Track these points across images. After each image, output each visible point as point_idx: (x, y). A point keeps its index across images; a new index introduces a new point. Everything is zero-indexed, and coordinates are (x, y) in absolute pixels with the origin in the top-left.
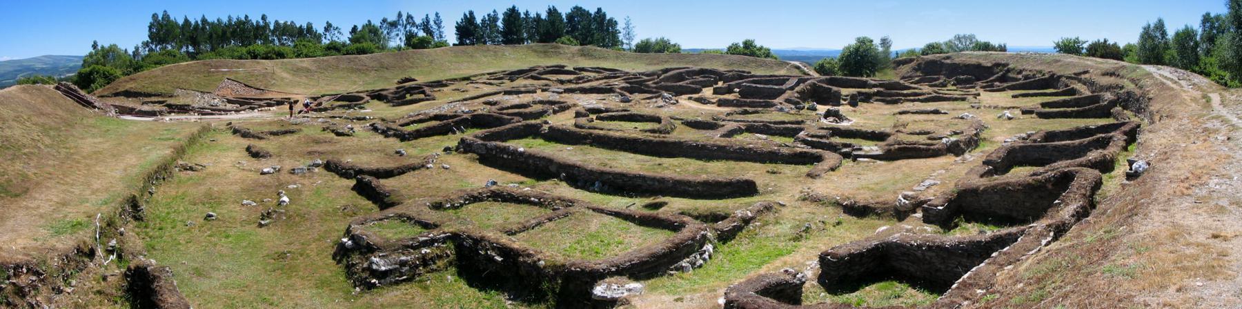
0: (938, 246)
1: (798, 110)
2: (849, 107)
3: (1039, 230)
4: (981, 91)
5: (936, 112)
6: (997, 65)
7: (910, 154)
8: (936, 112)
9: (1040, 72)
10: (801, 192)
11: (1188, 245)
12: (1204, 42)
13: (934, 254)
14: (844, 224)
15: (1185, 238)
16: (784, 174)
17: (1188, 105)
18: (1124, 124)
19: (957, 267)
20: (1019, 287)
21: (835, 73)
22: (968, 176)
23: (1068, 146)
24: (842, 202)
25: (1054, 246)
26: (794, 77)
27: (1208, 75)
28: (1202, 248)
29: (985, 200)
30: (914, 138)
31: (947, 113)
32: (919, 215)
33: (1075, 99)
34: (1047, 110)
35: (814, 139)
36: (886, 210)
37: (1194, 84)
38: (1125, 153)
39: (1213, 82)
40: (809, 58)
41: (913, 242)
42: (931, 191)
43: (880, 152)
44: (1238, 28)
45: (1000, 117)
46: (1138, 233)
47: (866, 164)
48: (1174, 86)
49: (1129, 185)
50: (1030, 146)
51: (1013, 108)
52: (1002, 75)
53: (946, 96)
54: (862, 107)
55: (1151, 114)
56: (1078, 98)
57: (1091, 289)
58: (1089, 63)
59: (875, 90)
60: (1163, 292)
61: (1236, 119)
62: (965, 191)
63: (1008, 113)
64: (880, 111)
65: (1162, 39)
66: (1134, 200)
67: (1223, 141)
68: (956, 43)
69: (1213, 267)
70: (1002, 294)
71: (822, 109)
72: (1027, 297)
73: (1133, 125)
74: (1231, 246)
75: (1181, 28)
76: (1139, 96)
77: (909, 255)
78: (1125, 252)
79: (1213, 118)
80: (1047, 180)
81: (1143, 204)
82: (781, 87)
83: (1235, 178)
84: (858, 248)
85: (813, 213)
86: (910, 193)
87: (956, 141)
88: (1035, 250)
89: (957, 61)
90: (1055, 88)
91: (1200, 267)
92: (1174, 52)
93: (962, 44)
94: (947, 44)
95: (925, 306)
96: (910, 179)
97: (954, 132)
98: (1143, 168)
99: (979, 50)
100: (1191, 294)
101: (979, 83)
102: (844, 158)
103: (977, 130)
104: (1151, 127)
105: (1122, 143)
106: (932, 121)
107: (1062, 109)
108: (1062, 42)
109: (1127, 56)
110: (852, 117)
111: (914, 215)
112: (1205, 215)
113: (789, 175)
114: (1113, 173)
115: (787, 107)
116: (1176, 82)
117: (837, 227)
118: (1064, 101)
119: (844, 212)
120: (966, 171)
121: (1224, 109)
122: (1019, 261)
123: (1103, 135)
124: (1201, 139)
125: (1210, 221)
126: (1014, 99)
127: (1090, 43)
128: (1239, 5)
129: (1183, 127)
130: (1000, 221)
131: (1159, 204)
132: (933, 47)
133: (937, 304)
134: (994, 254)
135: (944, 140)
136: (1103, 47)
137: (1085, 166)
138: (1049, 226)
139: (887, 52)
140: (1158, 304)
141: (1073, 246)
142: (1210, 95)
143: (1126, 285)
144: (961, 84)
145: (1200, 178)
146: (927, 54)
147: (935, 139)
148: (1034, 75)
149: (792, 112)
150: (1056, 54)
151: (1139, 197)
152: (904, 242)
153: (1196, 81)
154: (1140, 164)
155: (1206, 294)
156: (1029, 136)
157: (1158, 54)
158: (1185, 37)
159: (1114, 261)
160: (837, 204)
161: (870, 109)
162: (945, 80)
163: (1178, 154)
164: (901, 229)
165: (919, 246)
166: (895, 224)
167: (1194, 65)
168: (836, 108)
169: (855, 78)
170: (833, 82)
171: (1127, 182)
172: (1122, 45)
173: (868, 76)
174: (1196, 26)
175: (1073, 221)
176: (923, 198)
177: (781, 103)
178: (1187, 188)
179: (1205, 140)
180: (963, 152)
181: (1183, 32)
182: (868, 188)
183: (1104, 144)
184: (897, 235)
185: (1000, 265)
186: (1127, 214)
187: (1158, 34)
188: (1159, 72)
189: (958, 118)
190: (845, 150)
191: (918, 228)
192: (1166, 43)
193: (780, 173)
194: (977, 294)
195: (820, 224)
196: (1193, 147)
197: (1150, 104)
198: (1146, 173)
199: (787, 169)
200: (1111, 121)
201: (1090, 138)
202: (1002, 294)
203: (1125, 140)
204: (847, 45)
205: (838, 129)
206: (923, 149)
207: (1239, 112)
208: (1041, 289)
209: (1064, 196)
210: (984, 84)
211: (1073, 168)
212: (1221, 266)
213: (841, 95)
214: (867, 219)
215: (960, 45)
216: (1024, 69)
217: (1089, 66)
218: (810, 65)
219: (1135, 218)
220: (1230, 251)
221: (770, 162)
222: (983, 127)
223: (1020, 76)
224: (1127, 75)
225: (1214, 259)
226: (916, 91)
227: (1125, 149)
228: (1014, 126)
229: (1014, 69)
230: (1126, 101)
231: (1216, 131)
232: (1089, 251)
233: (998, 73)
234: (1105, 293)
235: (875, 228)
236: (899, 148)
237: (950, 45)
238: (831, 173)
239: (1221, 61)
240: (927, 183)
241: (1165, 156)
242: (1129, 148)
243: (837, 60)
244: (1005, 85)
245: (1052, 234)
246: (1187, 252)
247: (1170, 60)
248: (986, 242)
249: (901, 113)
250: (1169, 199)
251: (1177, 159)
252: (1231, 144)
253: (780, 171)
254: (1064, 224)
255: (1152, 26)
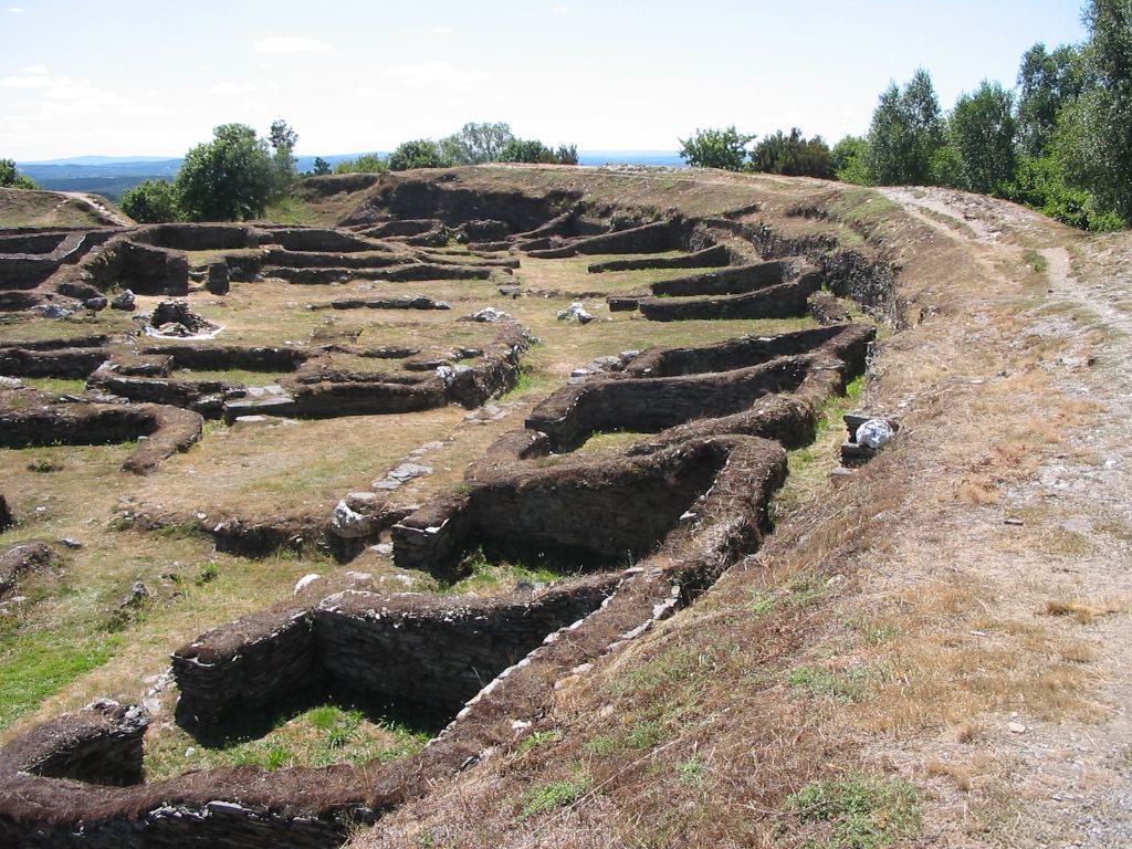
0: (427, 621)
1: (89, 311)
2: (208, 295)
3: (649, 580)
4: (522, 257)
5: (424, 305)
6: (557, 195)
7: (365, 403)
8: (424, 305)
9: (651, 211)
10: (115, 510)
11: (990, 627)
12: (1029, 120)
13: (418, 639)
14: (221, 578)
15: (982, 611)
16: (71, 469)
17: (989, 281)
18: (836, 331)
19: (469, 669)
20: (604, 713)
21: (171, 216)
22: (494, 455)
23: (711, 384)
24: (211, 525)
25: (681, 618)
26: (75, 230)
27: (1038, 202)
28: (1025, 636)
29: (531, 511)
30: (375, 366)
31: (447, 308)
32: (385, 547)
33: (727, 274)
34: (666, 300)
35: (134, 380)
36: (308, 536)
37: (1004, 229)
38: (840, 401)
39: (1051, 220)
40: (109, 182)
41: (371, 612)
42: (413, 491)
43: (286, 399)
44: (1118, 73)
45: (562, 318)
46: (869, 593)
47: (258, 429)
48: (955, 235)
49: (848, 476)
50: (628, 384)
51: (592, 295)
52: (567, 219)
53: (446, 267)
54: (239, 292)
55: (901, 305)
56: (735, 272)
57: (762, 724)
58: (758, 187)
59: (267, 249)
60: (927, 740)
61: (1111, 312)
62: (486, 489)
63: (580, 309)
64: (280, 301)
65: (927, 121)
66: (860, 514)
67: (1077, 370)
68: (468, 143)
69: (1052, 687)
70: (567, 730)
71: (147, 304)
72: (621, 738)
73: (858, 333)
74: (1097, 637)
75: (972, 89)
76: (871, 261)
77: (363, 641)
78: (838, 638)
79: (1051, 310)
80: (667, 465)
81: (881, 523)
82: (46, 256)
83: (1109, 463)
84: (257, 631)
85: (149, 559)
86: (366, 496)
87: (467, 373)
88: (639, 629)
89: (470, 184)
90: (683, 249)
91: (1018, 685)
92: (954, 151)
93: (480, 146)
94: (446, 144)
95: (399, 761)
96: (364, 463)
97: (462, 351)
98: (882, 437)
99: (518, 159)
100: (997, 752)
101: (518, 237)
102: (206, 419)
103: (512, 347)
104: (898, 337)
105: (832, 378)
106: (415, 325)
107: (698, 298)
108: (699, 141)
109: (844, 167)
110: (217, 318)
111: (375, 548)
112: (1030, 555)
113: (82, 471)
114: (812, 449)
115: (65, 305)
116: (958, 226)
117: (206, 585)
118: (704, 279)
119: (219, 549)
120: (489, 443)
121: (1081, 287)
122: (604, 653)
123: (790, 359)
124: (1021, 364)
125: (1041, 572)
126: (593, 275)
127: (760, 139)
128: (1120, 18)
129: (977, 335)
130: (563, 561)
131: (918, 524)
132: (418, 152)
133: (425, 756)
134: (550, 638)
135: (441, 371)
136: (790, 148)
137: (749, 431)
138: (670, 572)
139: (285, 159)
140: (917, 768)
141: (721, 621)
142: (1046, 253)
143: (841, 718)
144: (477, 241)
145: (1017, 461)
146: (404, 168)
147: (420, 368)
148: (636, 219)
149: (78, 316)
150: (685, 169)
151: (870, 507)
152: (352, 612)
153: (1008, 219)
154: (873, 428)
155: (1033, 754)
156: (626, 361)
157: (916, 158)
158: (983, 110)
159: (814, 658)
160: (201, 531)
161: (256, 296)
162: (443, 231)
163: (965, 403)
164: (346, 581)
165: (386, 622)
166: (330, 570)
167: (1003, 180)
168: (179, 300)
169: (218, 224)
170: (165, 237)
171: (845, 471)
172: (832, 142)
173: (248, 217)
174: (1009, 80)
175: (722, 561)
176: (393, 507)
177: (49, 297)
178: (987, 488)
179: (1031, 368)
180: (483, 399)
181: (978, 101)
182: (268, 485)
183: (790, 379)
184: (335, 597)
185: (561, 662)
186: (844, 547)
187: (916, 111)
188: (919, 202)
189: (472, 319)
190: (206, 399)
191: (382, 579)
192: (935, 131)
193: (61, 469)
194: (514, 731)
195: (166, 584)
196: (1003, 383)
197: (898, 281)
198: (888, 450)
199: (78, 458)
200: (808, 324)
201: (761, 366)
202: (567, 730)
203: (839, 370)
204: (195, 146)
205: (188, 350)
206: (395, 392)
207: (1120, 293)
208: (651, 719)
209: (702, 503)
210: (529, 241)
211: (723, 437)
212: (1072, 688)
213: (189, 267)
214: (271, 559)
215: (475, 149)
216: (614, 206)
217: (757, 194)
218: (112, 198)
219: (862, 556)
220: (1095, 650)
221: (37, 444)
222: (524, 342)
223: (606, 222)
224: (844, 213)
225: (1054, 668)
226: (380, 254)
227: (840, 390)
228: (594, 339)
229: (593, 204)
230: (842, 276)
231: (1060, 343)
232: (758, 633)
233: (558, 214)
234: (794, 733)
235: (291, 579)
236: (334, 389)
237: (452, 146)
238: (180, 457)
239: (1071, 166)
240: (403, 471)
241: (934, 407)
242: (849, 388)
243: (174, 186)
244: (575, 242)
245: (676, 591)
246: (987, 645)
247: (945, 172)
248: (534, 610)
249: (339, 306)
250: (942, 512)
251: (963, 415)
252: (1097, 375)
253: (59, 463)
254: (702, 568)
255: (902, 91)
